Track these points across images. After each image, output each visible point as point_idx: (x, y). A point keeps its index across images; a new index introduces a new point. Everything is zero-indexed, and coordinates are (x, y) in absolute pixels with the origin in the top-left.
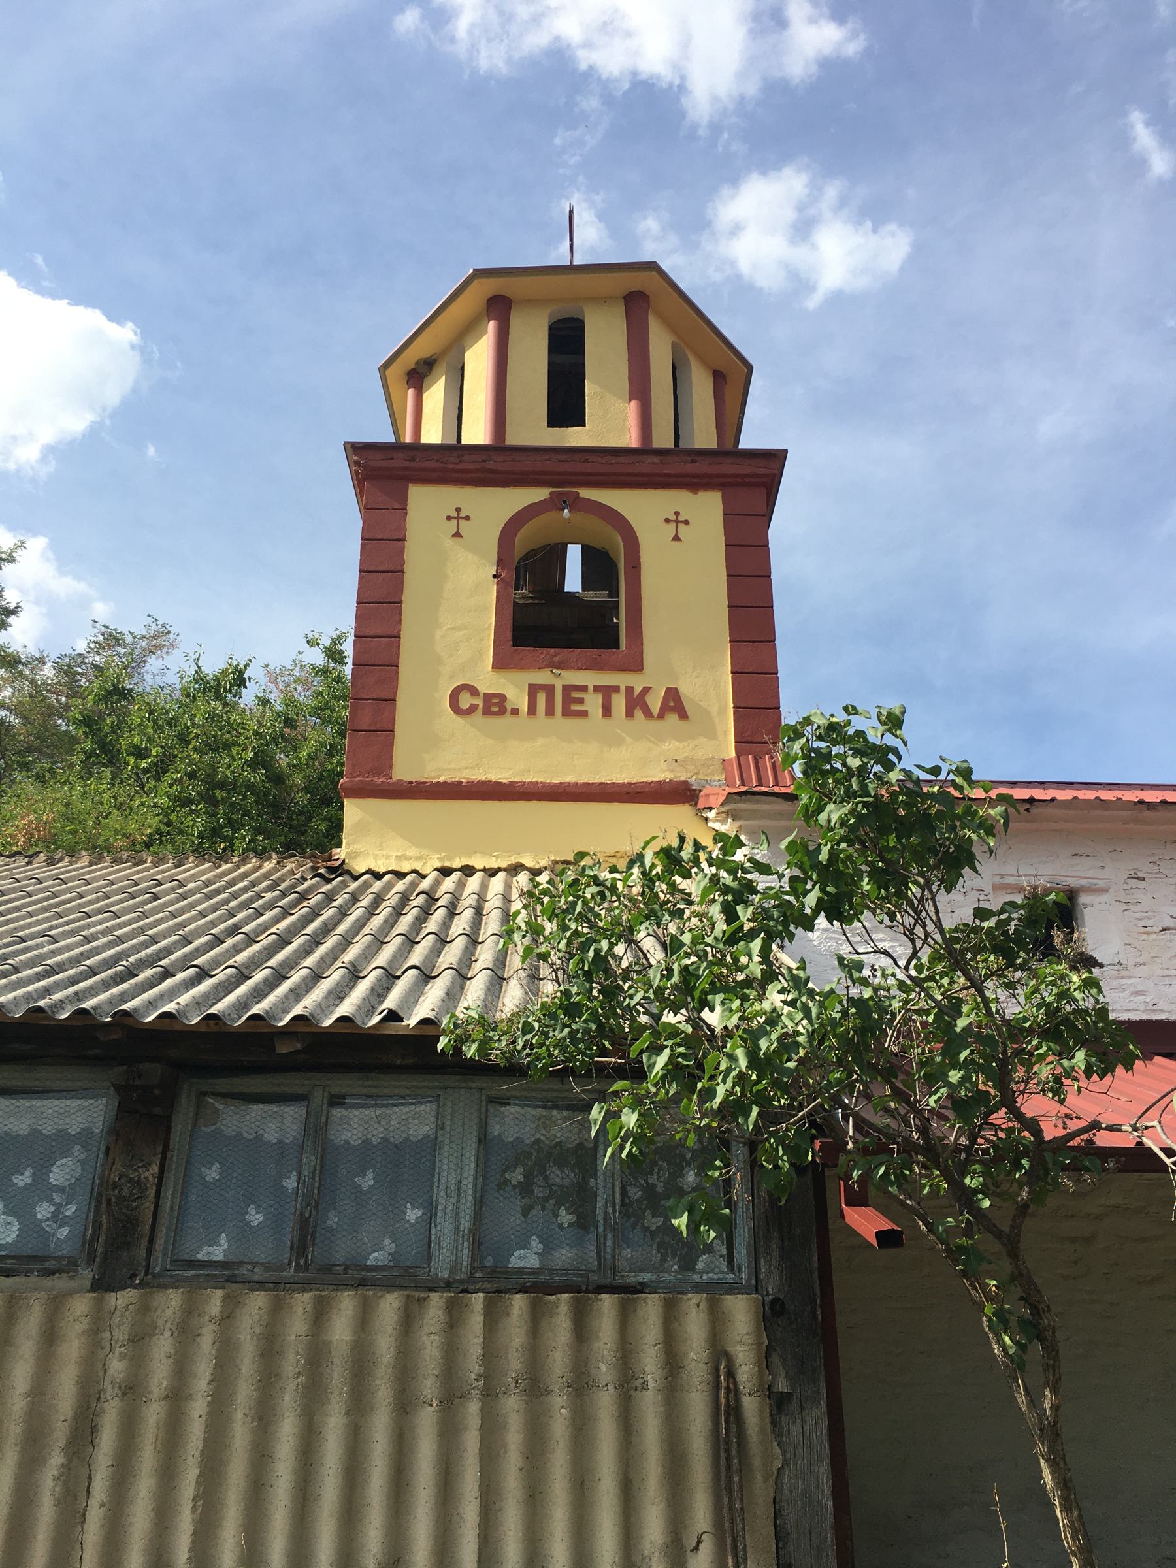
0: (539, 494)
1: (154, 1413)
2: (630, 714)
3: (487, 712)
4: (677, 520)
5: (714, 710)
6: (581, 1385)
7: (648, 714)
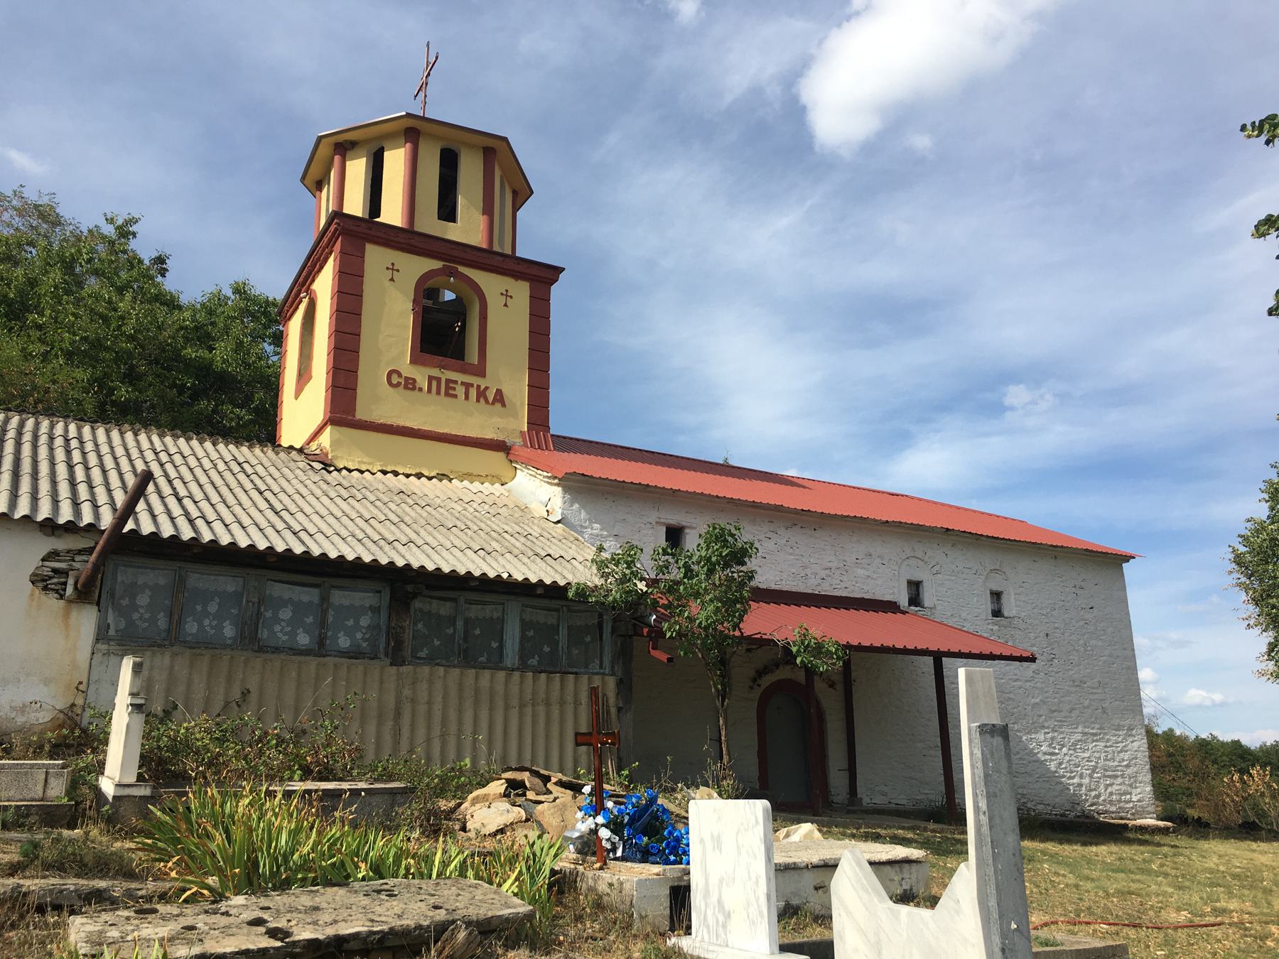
0: (436, 264)
1: (422, 708)
2: (478, 400)
3: (406, 387)
4: (506, 295)
5: (518, 404)
6: (562, 703)
7: (487, 401)
